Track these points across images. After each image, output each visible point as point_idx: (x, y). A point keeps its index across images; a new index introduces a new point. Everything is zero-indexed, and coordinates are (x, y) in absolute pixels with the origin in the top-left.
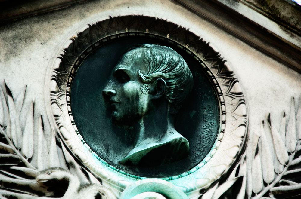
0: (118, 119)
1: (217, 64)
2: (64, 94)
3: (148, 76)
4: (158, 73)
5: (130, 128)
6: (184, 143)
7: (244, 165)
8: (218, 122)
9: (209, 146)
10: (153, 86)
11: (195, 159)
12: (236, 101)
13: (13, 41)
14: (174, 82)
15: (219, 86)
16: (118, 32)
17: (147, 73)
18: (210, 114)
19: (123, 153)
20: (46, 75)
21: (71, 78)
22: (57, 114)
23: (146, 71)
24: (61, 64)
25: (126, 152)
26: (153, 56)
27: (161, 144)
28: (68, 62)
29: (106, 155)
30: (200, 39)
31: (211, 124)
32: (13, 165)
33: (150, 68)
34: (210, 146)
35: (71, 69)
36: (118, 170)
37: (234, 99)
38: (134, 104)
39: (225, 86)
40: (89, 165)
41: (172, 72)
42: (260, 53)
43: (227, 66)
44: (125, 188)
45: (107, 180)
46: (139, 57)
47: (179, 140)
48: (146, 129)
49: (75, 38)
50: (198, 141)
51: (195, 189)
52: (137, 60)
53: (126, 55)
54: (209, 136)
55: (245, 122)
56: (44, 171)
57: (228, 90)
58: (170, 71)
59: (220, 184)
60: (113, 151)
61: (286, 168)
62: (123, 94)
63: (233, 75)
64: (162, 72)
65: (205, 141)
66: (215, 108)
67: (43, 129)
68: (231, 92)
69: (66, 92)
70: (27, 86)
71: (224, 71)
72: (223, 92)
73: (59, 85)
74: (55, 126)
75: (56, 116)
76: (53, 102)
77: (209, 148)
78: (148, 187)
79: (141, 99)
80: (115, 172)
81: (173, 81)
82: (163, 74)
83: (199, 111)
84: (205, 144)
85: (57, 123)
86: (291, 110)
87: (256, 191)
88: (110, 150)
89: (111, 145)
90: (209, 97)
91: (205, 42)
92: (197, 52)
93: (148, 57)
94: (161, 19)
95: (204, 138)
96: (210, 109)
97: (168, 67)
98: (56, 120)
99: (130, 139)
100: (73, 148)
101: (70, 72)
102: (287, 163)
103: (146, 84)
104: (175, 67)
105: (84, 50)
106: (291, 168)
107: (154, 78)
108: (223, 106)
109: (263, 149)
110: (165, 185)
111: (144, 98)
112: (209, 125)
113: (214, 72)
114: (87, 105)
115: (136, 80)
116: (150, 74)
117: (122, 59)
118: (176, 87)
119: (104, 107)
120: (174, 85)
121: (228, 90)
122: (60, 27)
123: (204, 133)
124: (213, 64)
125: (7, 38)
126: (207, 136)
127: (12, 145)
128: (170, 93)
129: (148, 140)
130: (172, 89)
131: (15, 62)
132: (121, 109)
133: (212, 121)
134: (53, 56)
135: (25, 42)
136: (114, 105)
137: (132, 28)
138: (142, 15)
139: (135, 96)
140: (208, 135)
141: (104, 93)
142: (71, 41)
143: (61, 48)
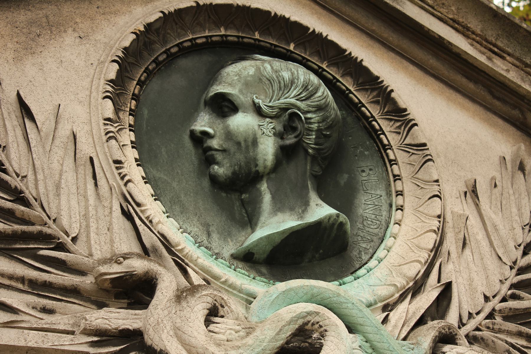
0: (222, 179)
1: (378, 95)
2: (126, 128)
3: (270, 104)
4: (288, 100)
5: (243, 197)
6: (342, 224)
7: (449, 263)
8: (389, 194)
9: (380, 234)
10: (280, 123)
11: (359, 254)
12: (417, 159)
13: (29, 29)
14: (315, 118)
15: (384, 133)
16: (209, 33)
17: (269, 100)
18: (373, 181)
19: (236, 240)
20: (93, 90)
21: (134, 102)
22: (119, 159)
23: (266, 97)
24: (119, 73)
25: (240, 239)
26: (276, 72)
27: (306, 223)
28: (128, 72)
29: (207, 242)
30: (347, 53)
31: (376, 197)
32: (44, 247)
33: (273, 91)
34: (381, 233)
35: (133, 87)
36: (233, 267)
37: (413, 154)
38: (249, 154)
39: (395, 134)
40: (187, 253)
41: (311, 101)
42: (441, 84)
43: (397, 100)
44: (255, 298)
45: (221, 282)
46: (250, 73)
47: (335, 217)
49: (140, 31)
51: (376, 303)
52: (249, 79)
53: (226, 71)
54: (378, 216)
55: (438, 191)
57: (400, 140)
58: (308, 98)
59: (414, 296)
60: (218, 236)
61: (514, 271)
62: (229, 135)
63: (409, 114)
64: (294, 98)
65: (371, 225)
66: (380, 170)
67: (96, 185)
68: (405, 142)
69: (128, 125)
70: (60, 105)
71: (390, 109)
72: (392, 143)
73: (117, 110)
74: (116, 182)
75: (117, 162)
77: (381, 236)
78: (301, 294)
79: (261, 144)
80: (230, 271)
81: (314, 116)
82: (298, 102)
83: (353, 175)
84: (372, 230)
85: (120, 174)
86: (502, 177)
87: (474, 312)
88: (212, 233)
89: (213, 225)
90: (368, 152)
91: (357, 58)
93: (267, 73)
94: (281, 15)
95: (369, 219)
96: (371, 172)
97: (303, 90)
98: (117, 168)
99: (244, 216)
100: (153, 221)
101: (133, 90)
102: (515, 263)
103: (268, 120)
104: (315, 93)
105: (154, 55)
107: (284, 110)
108: (394, 167)
109: (472, 239)
110: (331, 290)
111: (267, 142)
112: (374, 198)
114: (164, 153)
115: (249, 112)
116: (274, 101)
117: (219, 77)
118: (319, 126)
119: (193, 159)
120: (315, 123)
121: (400, 140)
122: (111, 13)
123: (367, 211)
124: (370, 97)
125: (16, 22)
126: (373, 216)
127: (40, 209)
128: (310, 137)
129: (280, 216)
130: (312, 131)
131: (34, 64)
132: (225, 161)
134: (102, 59)
135: (49, 32)
136: (212, 155)
137: (231, 28)
138: (250, 6)
139: (250, 140)
140: (375, 216)
141: (192, 134)
142: (134, 36)
143: (117, 45)
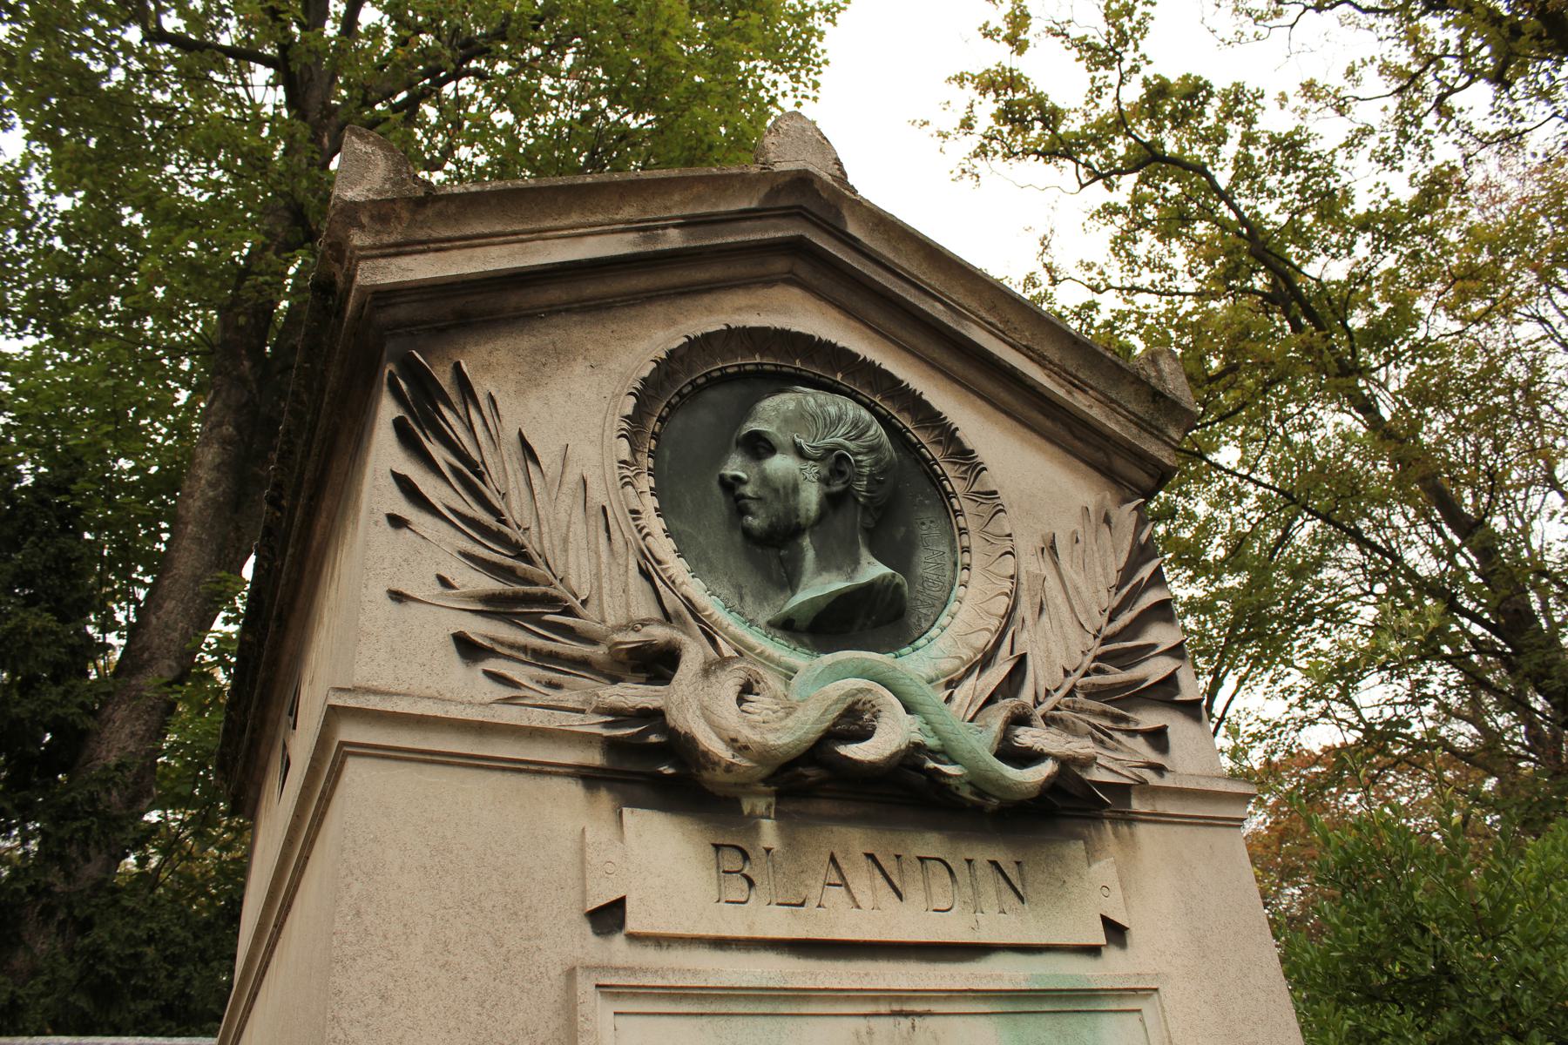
6: (898, 586)
8: (953, 551)
12: (986, 509)
21: (653, 442)
24: (637, 407)
35: (653, 424)
48: (818, 554)
50: (920, 588)
51: (938, 679)
56: (619, 629)
58: (858, 437)
59: (982, 671)
61: (1098, 641)
62: (765, 480)
73: (634, 451)
75: (633, 512)
76: (627, 483)
85: (637, 526)
87: (1051, 688)
92: (899, 412)
98: (634, 519)
102: (1099, 631)
103: (811, 462)
106: (1106, 641)
107: (829, 451)
113: (934, 452)
122: (627, 338)
127: (544, 567)
129: (826, 576)
133: (941, 548)
136: (746, 505)
